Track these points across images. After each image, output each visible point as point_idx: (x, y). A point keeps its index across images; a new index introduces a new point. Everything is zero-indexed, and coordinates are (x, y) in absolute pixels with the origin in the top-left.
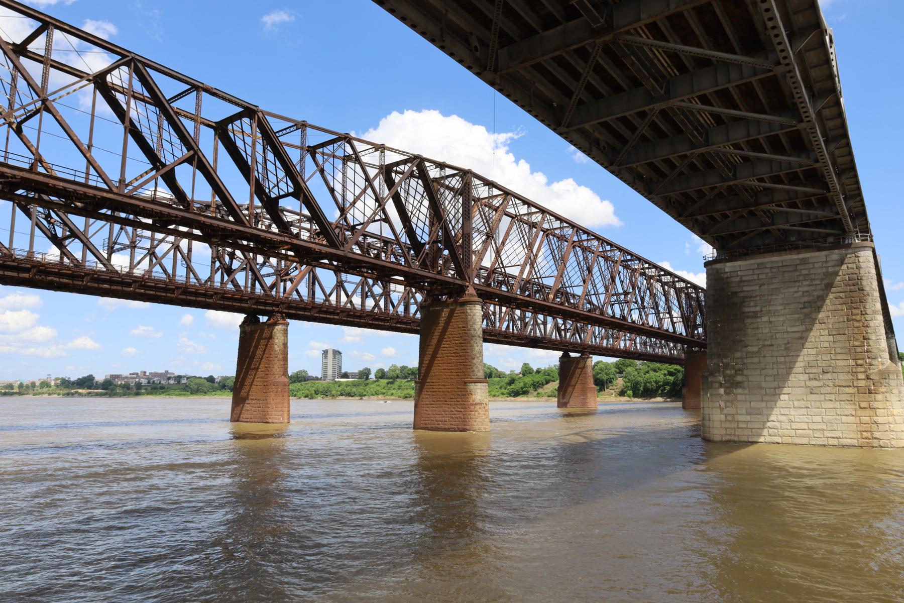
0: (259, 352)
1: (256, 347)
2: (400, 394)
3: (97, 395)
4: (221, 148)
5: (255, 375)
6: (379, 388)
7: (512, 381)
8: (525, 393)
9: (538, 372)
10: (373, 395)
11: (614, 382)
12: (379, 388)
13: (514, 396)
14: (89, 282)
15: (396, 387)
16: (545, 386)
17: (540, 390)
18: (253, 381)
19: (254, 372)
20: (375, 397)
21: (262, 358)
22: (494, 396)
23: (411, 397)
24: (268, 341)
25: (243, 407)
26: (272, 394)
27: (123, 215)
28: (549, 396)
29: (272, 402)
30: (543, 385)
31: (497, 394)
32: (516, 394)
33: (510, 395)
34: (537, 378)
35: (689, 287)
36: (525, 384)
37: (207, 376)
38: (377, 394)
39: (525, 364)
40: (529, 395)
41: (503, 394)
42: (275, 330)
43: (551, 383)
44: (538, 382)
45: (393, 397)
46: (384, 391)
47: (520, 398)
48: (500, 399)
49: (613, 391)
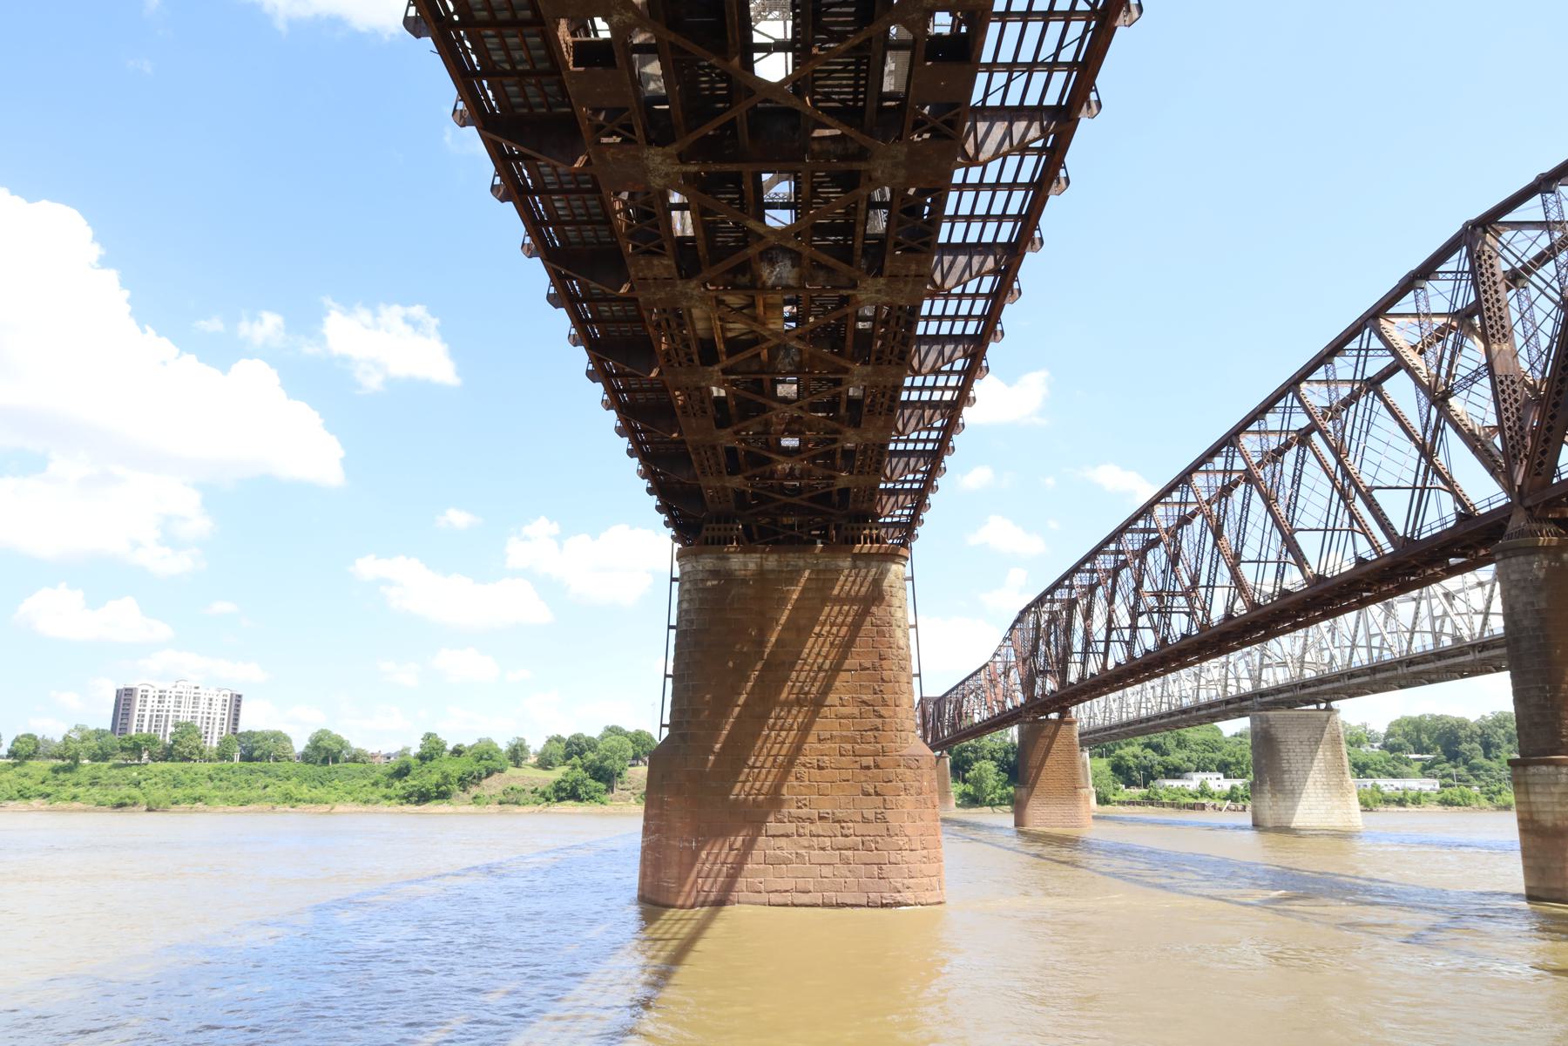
0: (816, 650)
1: (800, 629)
2: (100, 798)
3: (80, 810)
4: (1076, 44)
5: (805, 729)
6: (27, 782)
7: (402, 772)
8: (443, 796)
9: (457, 752)
10: (10, 799)
11: (625, 775)
12: (27, 782)
13: (417, 803)
14: (859, 268)
15: (85, 780)
16: (484, 782)
17: (474, 791)
18: (797, 749)
19: (798, 717)
20: (21, 804)
21: (837, 668)
22: (367, 802)
23: (135, 804)
24: (866, 612)
25: (749, 846)
26: (907, 801)
27: (525, 172)
28: (501, 803)
29: (909, 828)
30: (480, 778)
31: (372, 797)
32: (423, 797)
33: (407, 798)
34: (455, 768)
35: (1052, 596)
36: (446, 777)
37: (632, 730)
38: (23, 795)
39: (428, 736)
40: (453, 800)
41: (387, 797)
42: (891, 577)
43: (496, 775)
44: (471, 774)
45: (76, 805)
46: (42, 788)
47: (432, 807)
48: (386, 809)
49: (628, 793)
